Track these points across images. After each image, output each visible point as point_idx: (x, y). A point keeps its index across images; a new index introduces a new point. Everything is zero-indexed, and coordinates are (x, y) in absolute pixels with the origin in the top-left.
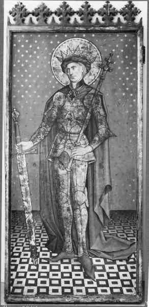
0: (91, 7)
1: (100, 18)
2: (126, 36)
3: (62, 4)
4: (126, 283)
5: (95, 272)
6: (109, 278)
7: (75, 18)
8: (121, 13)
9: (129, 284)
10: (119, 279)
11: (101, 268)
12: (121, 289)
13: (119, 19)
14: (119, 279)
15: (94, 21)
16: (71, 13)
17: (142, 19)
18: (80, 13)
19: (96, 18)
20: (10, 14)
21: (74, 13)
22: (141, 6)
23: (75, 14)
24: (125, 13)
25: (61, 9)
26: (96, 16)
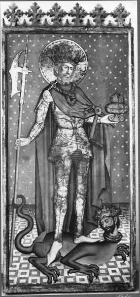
0: (61, 8)
1: (91, 19)
2: (19, 36)
3: (33, 5)
4: (125, 271)
5: (129, 267)
6: (123, 274)
7: (46, 19)
8: (91, 14)
9: (128, 272)
10: (109, 275)
11: (104, 272)
12: (120, 277)
13: (89, 21)
14: (109, 275)
15: (64, 22)
16: (63, 14)
17: (130, 19)
18: (29, 14)
19: (109, 20)
20: (5, 15)
21: (23, 14)
22: (131, 8)
23: (24, 15)
24: (30, 14)
25: (53, 11)
26: (88, 17)
